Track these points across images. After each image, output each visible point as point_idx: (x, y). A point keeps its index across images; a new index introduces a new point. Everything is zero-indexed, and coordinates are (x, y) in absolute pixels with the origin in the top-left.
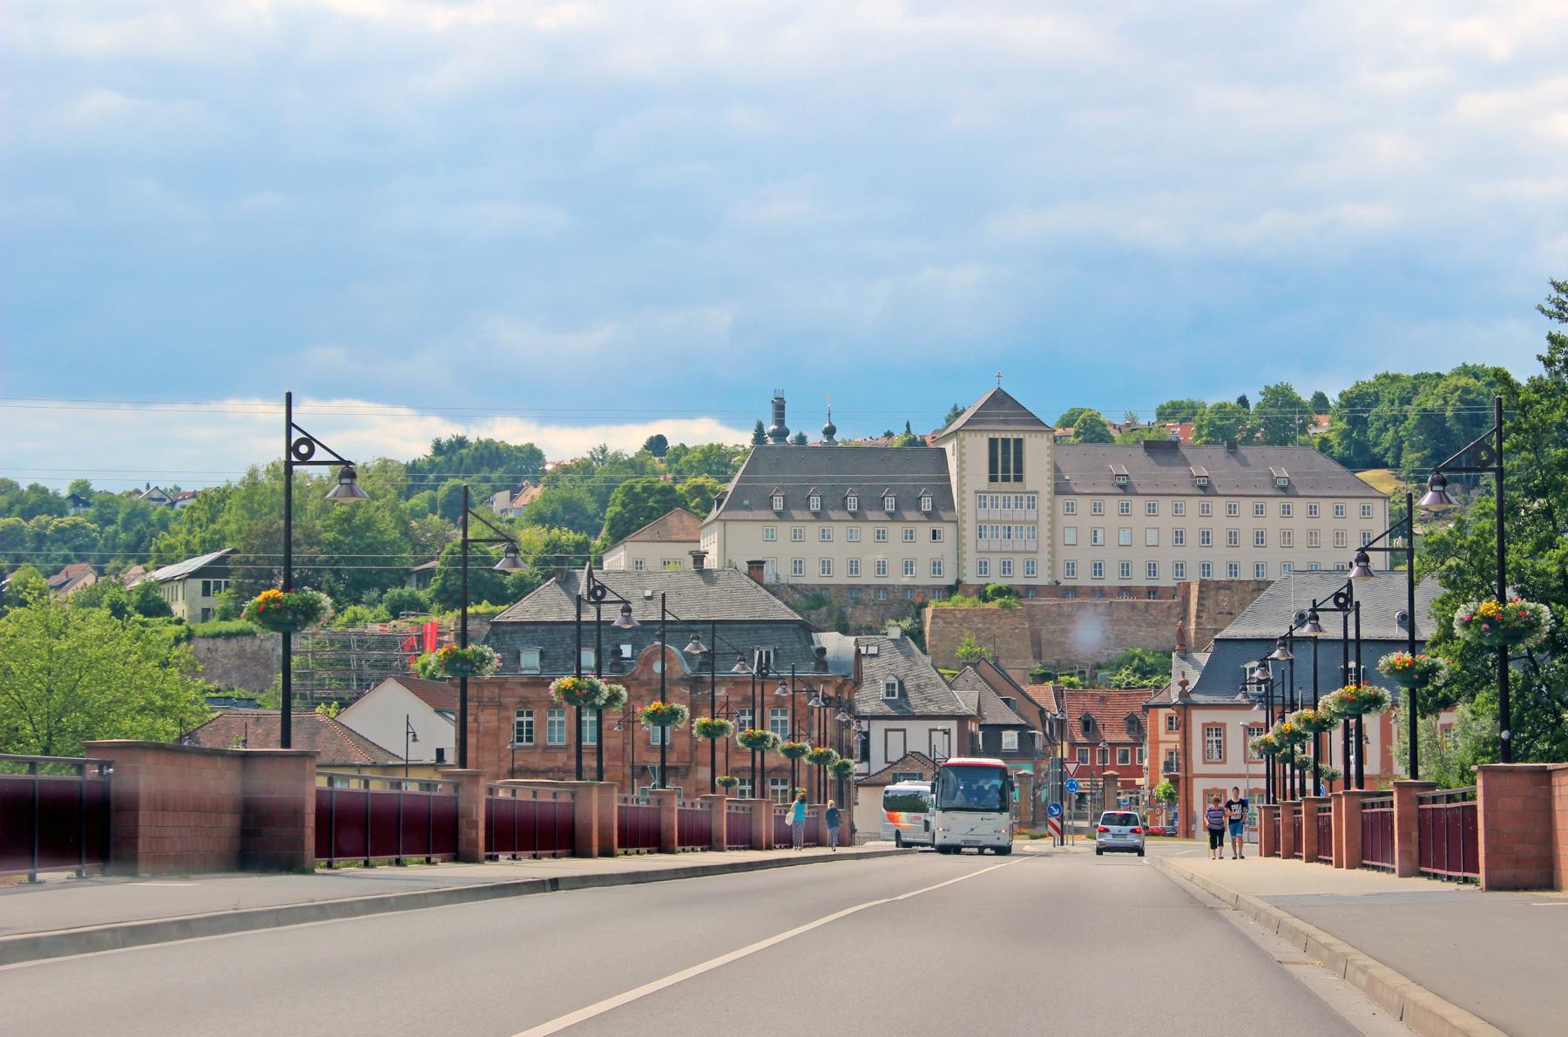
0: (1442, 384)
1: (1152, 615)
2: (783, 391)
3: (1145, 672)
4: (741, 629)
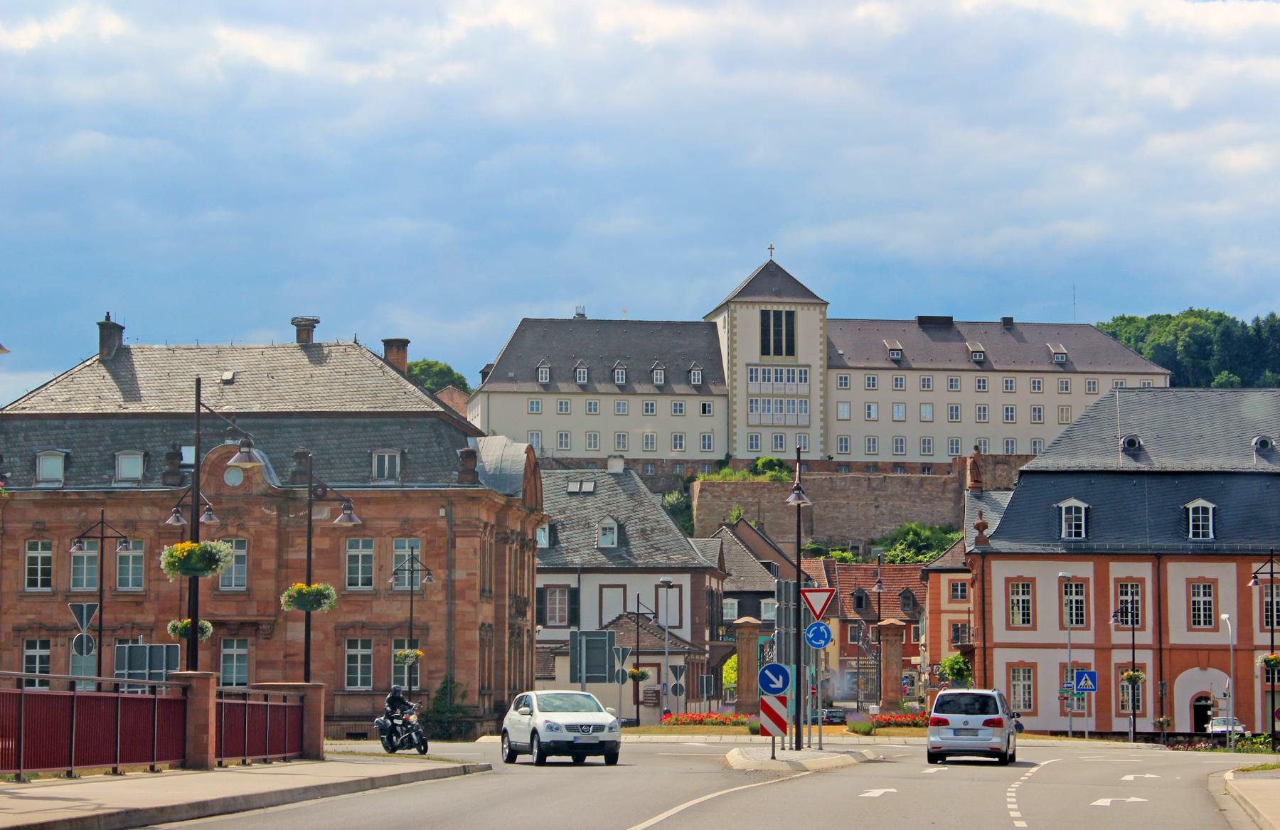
0: (1173, 323)
1: (926, 490)
2: (584, 308)
3: (920, 547)
4: (357, 425)
